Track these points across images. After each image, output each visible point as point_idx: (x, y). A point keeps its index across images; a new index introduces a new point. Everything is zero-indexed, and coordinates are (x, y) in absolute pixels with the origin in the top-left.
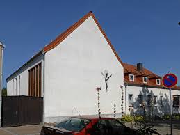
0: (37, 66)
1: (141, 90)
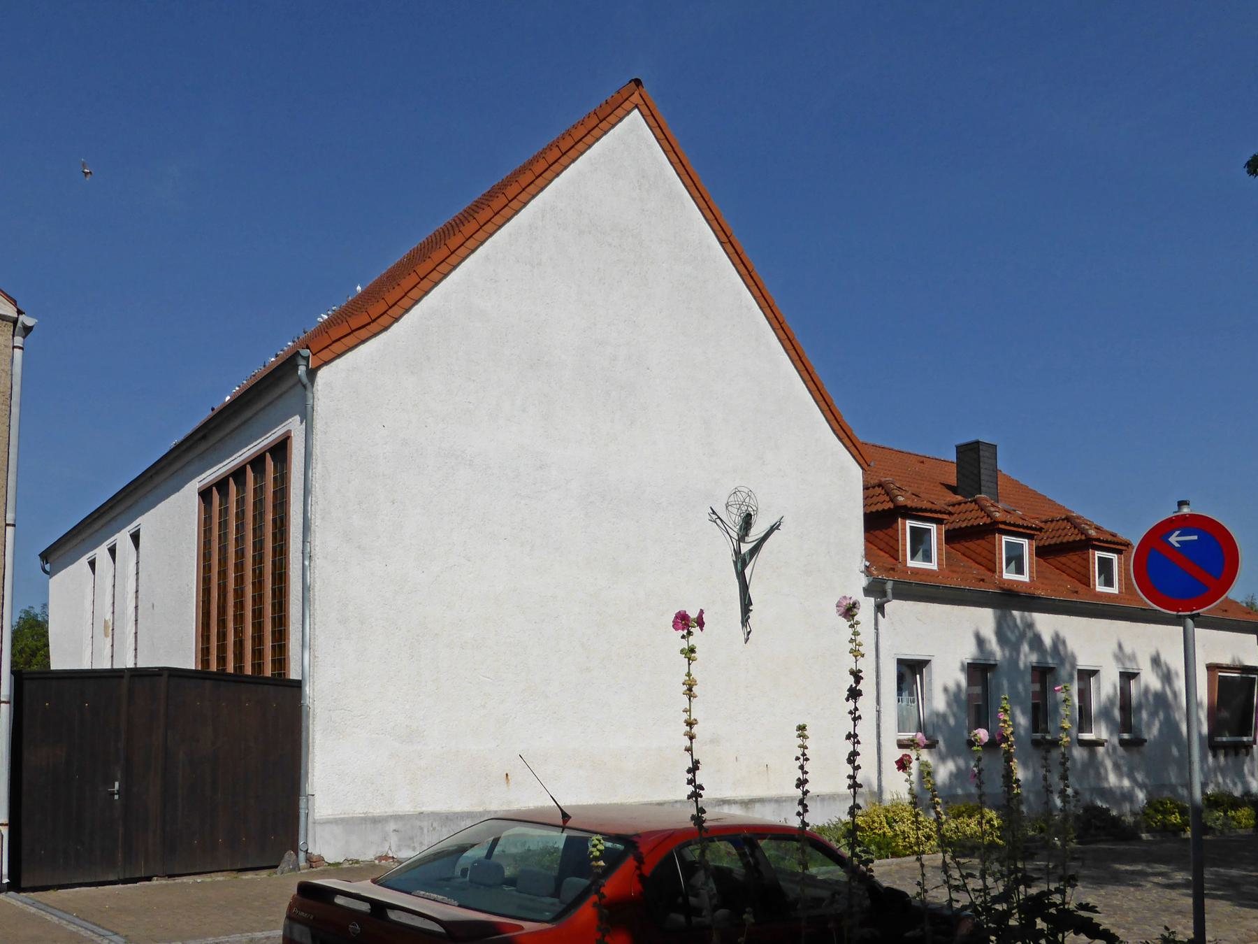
0: (257, 462)
1: (989, 633)
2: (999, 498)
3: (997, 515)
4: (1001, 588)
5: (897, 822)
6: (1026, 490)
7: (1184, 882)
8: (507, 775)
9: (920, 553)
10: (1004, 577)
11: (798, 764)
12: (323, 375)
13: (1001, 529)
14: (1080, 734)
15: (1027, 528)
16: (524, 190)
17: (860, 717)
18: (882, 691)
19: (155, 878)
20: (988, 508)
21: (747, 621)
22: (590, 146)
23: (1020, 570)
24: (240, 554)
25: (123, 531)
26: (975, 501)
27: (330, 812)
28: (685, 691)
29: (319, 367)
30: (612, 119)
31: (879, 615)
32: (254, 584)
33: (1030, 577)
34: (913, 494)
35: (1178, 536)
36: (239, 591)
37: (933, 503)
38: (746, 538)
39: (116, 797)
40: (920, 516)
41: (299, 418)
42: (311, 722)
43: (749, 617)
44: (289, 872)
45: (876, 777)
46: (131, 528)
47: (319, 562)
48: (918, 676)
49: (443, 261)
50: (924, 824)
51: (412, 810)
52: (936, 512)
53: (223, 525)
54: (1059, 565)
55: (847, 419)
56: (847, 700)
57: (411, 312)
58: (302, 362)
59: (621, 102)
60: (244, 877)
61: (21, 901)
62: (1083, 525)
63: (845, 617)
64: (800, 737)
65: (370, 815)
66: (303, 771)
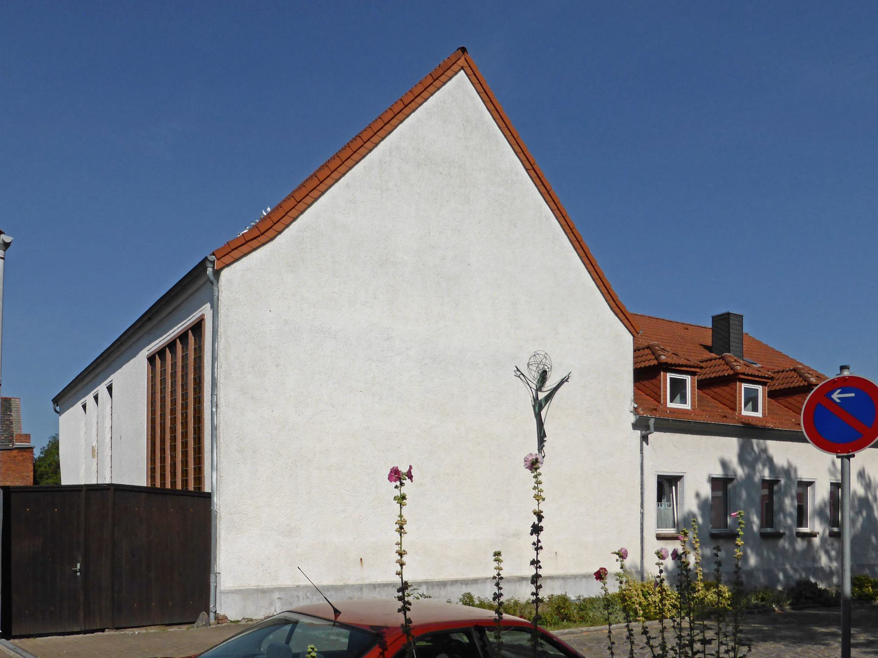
0: (183, 337)
1: (733, 457)
2: (744, 355)
3: (739, 368)
4: (743, 423)
5: (650, 595)
6: (767, 347)
7: (865, 641)
8: (361, 559)
9: (678, 397)
10: (742, 414)
11: (495, 581)
12: (225, 274)
13: (741, 378)
14: (797, 529)
15: (762, 377)
16: (375, 134)
17: (541, 548)
18: (645, 498)
19: (107, 630)
20: (732, 363)
21: (542, 448)
22: (426, 100)
23: (755, 409)
24: (174, 402)
25: (102, 385)
26: (723, 358)
27: (231, 585)
28: (397, 529)
29: (222, 269)
30: (443, 78)
31: (644, 443)
32: (182, 423)
33: (763, 413)
34: (673, 354)
35: (839, 393)
36: (173, 429)
37: (689, 360)
38: (543, 388)
39: (78, 574)
40: (681, 370)
41: (210, 305)
42: (218, 522)
43: (544, 446)
44: (202, 627)
45: (640, 561)
46: (106, 382)
47: (223, 408)
48: (674, 488)
49: (315, 188)
50: (671, 596)
51: (291, 584)
52: (690, 366)
53: (163, 381)
54: (787, 404)
55: (622, 299)
56: (532, 534)
57: (290, 227)
58: (209, 265)
59: (451, 65)
60: (169, 630)
61: (6, 647)
62: (806, 375)
63: (531, 470)
64: (496, 561)
65: (260, 587)
66: (212, 557)
